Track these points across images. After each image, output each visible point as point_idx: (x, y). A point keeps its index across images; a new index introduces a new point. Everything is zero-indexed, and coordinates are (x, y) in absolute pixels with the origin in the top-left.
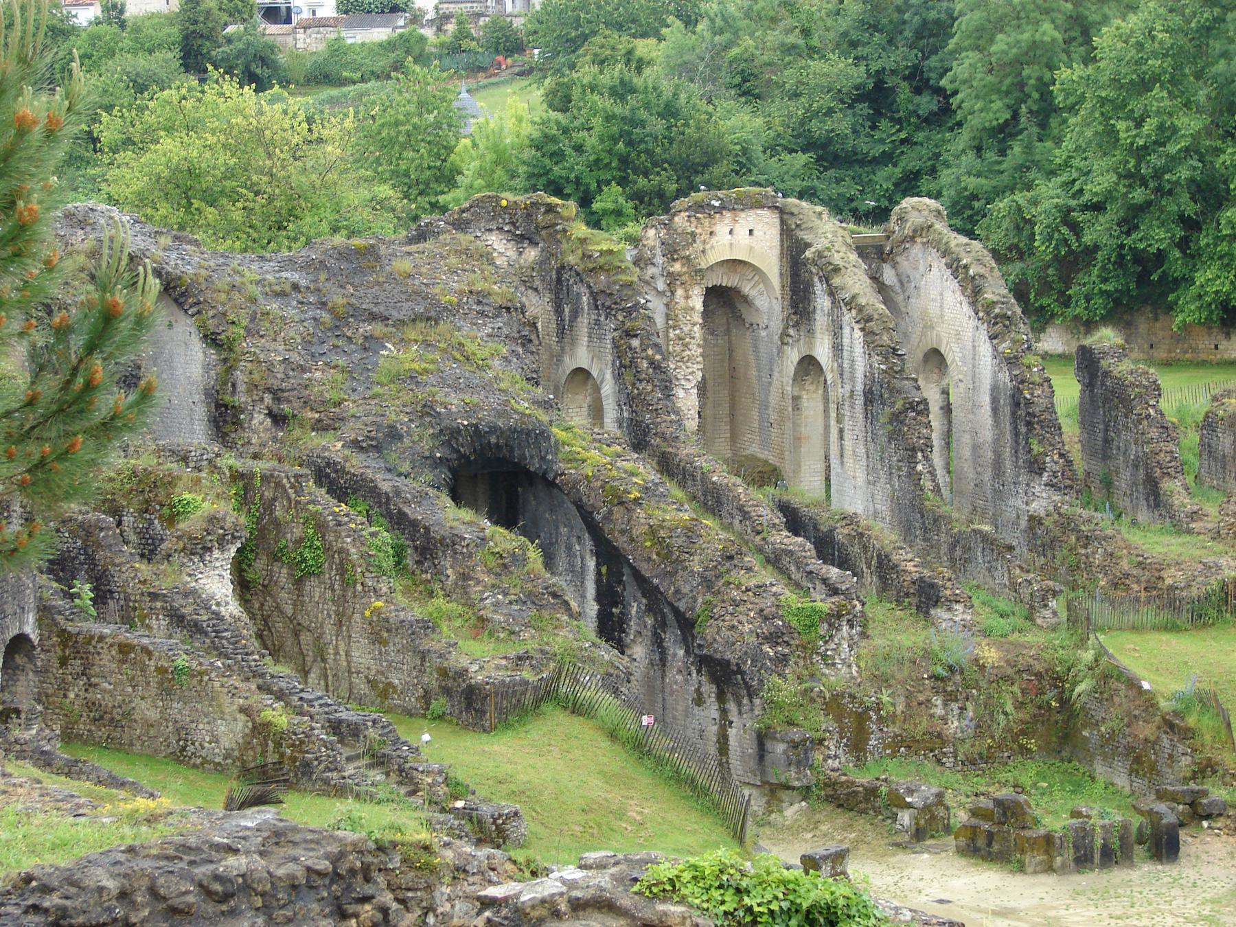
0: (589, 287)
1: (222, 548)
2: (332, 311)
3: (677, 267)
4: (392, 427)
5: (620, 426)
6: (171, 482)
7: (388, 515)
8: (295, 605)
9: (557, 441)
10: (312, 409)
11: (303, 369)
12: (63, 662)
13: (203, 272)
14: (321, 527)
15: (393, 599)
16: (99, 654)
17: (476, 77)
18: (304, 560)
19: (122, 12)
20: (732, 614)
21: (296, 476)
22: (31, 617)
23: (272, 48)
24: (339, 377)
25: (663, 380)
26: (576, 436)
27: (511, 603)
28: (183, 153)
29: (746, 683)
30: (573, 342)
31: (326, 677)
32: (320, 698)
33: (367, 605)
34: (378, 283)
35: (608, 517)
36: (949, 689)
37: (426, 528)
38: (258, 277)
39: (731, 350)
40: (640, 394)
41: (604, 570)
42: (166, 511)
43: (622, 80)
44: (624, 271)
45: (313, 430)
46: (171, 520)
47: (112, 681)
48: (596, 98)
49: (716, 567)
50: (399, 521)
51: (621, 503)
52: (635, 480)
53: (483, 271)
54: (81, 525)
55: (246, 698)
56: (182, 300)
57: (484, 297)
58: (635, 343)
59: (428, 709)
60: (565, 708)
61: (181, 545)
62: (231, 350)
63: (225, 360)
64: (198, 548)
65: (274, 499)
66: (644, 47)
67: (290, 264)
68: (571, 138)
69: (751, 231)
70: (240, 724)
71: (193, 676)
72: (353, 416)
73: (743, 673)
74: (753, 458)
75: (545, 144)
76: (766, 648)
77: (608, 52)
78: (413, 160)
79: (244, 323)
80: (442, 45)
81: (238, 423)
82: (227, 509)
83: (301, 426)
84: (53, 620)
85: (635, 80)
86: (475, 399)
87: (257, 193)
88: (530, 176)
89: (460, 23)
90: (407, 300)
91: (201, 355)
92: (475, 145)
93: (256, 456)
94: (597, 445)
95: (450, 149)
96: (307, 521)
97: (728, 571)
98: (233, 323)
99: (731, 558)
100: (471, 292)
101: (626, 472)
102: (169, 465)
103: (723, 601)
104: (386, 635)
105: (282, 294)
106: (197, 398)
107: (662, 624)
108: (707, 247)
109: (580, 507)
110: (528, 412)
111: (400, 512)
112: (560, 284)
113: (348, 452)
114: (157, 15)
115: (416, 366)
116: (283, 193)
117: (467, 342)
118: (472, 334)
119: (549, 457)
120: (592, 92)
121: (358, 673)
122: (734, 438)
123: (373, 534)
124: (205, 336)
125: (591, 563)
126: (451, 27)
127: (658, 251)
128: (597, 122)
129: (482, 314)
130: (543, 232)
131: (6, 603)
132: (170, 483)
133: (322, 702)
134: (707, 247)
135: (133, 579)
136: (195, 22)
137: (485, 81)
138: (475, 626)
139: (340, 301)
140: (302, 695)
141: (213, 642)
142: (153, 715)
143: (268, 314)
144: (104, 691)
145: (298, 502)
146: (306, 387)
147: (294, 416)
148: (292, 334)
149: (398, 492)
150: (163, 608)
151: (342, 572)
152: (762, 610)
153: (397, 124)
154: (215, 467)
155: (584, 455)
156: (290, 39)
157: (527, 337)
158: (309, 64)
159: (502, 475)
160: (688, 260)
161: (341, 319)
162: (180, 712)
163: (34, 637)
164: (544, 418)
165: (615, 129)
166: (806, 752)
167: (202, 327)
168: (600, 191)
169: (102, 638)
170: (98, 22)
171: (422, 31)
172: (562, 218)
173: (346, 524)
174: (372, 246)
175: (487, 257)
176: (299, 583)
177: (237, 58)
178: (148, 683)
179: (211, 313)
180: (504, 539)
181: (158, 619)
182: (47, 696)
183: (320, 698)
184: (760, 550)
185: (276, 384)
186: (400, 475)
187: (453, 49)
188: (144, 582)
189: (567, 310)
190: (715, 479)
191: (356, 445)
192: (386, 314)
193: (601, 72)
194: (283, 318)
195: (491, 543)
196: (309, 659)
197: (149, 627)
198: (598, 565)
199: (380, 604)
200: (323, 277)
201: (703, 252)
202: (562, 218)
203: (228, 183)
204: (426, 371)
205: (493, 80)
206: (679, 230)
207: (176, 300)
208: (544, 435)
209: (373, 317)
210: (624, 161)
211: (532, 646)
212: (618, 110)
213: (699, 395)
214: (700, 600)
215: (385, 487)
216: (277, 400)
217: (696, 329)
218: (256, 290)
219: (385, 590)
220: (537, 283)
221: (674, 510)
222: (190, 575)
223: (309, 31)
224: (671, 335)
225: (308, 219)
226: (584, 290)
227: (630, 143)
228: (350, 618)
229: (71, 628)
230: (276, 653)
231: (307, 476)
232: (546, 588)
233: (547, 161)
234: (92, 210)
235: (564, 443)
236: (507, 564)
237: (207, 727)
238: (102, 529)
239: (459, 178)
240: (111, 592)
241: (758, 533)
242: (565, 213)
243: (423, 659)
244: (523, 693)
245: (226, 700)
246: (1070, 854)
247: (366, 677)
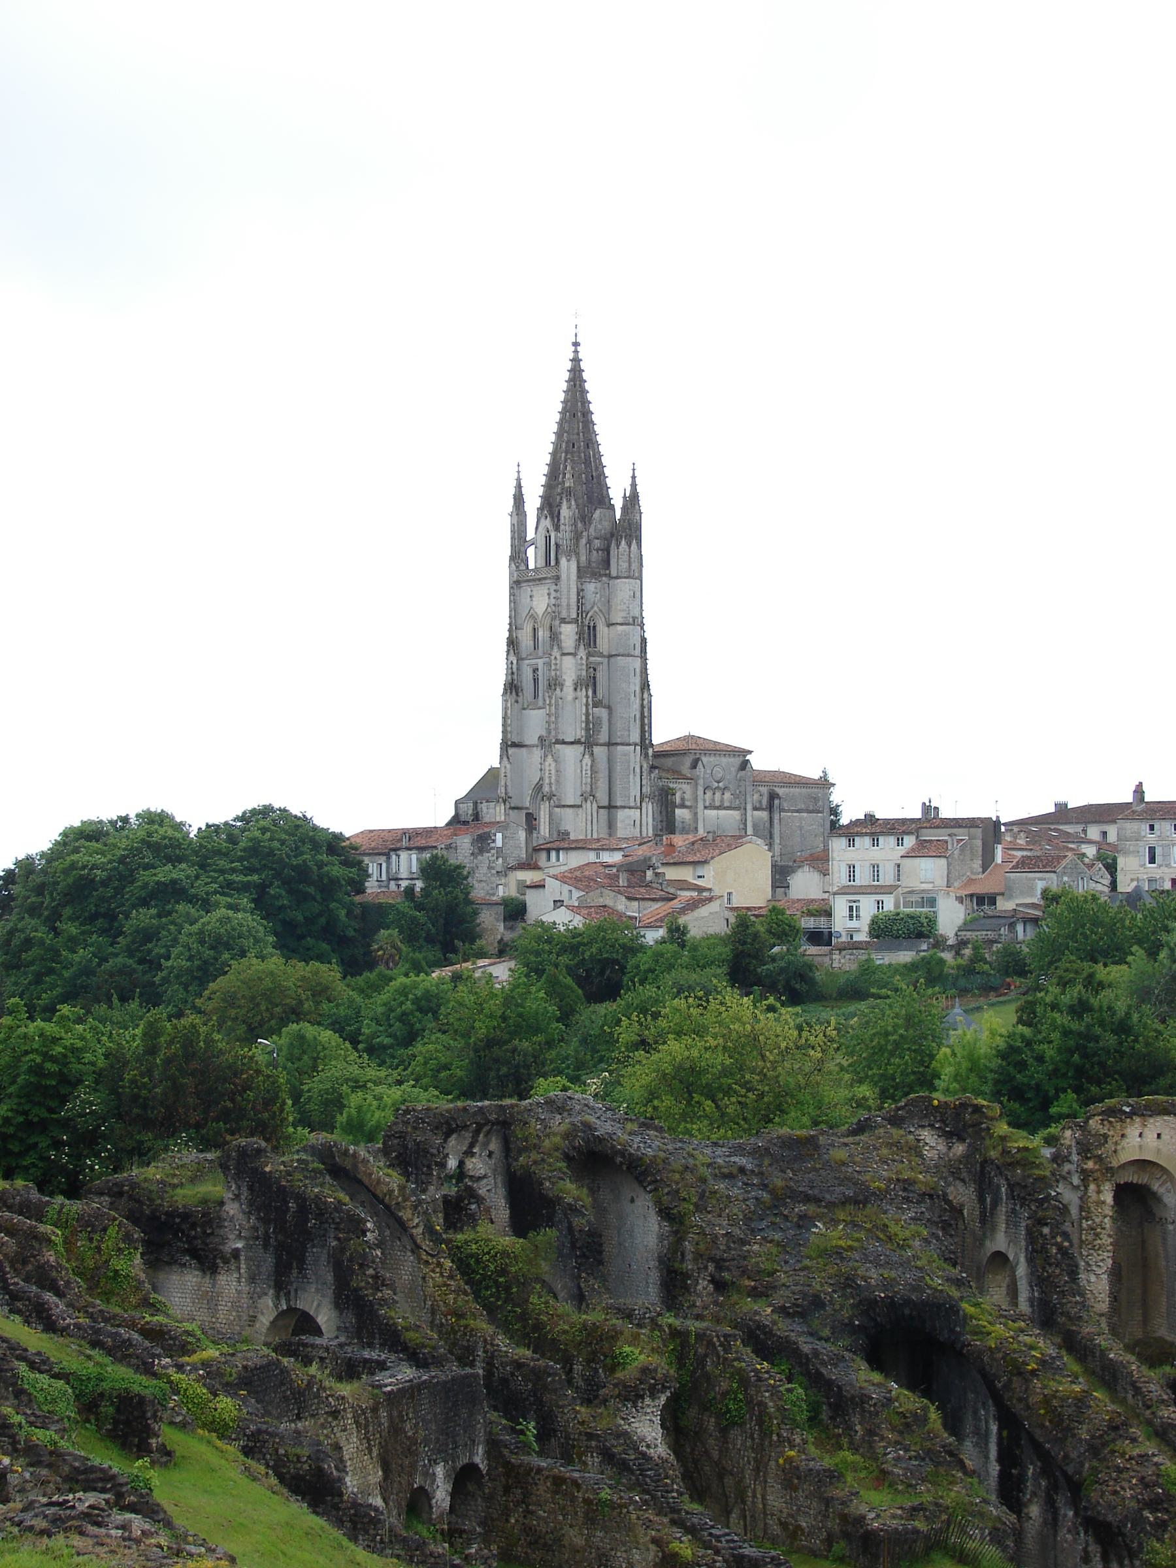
0: (1007, 1179)
1: (653, 1397)
2: (772, 1192)
3: (1090, 1165)
4: (816, 1296)
5: (1032, 1306)
6: (614, 1336)
7: (807, 1374)
8: (720, 1451)
9: (965, 1315)
10: (749, 1278)
11: (744, 1242)
12: (507, 1490)
13: (662, 1154)
14: (744, 1382)
15: (806, 1451)
16: (536, 1484)
17: (987, 996)
18: (729, 1411)
19: (684, 933)
20: (1115, 1480)
21: (725, 1336)
22: (480, 1450)
23: (810, 967)
24: (774, 1250)
25: (1069, 1265)
26: (983, 1311)
27: (910, 1458)
28: (687, 1053)
29: (1126, 1545)
30: (994, 1228)
31: (745, 1517)
32: (728, 1534)
33: (782, 1454)
34: (814, 1169)
35: (1008, 1386)
37: (839, 1387)
38: (709, 1161)
39: (1143, 1242)
40: (1049, 1277)
41: (1005, 1434)
42: (609, 1361)
43: (1080, 1000)
44: (1038, 1166)
45: (749, 1296)
46: (612, 1369)
47: (547, 1509)
48: (1056, 1015)
49: (1101, 1436)
50: (816, 1381)
51: (1020, 1374)
52: (1033, 1353)
53: (910, 1162)
54: (533, 1370)
55: (658, 1530)
56: (642, 1178)
57: (910, 1184)
58: (1046, 1230)
59: (830, 1551)
60: (953, 1557)
61: (617, 1391)
62: (682, 1223)
63: (676, 1232)
64: (632, 1395)
65: (706, 1355)
66: (1102, 972)
67: (739, 1150)
68: (1032, 1050)
69: (1159, 1136)
70: (652, 1554)
71: (613, 1508)
72: (784, 1285)
73: (1124, 1535)
74: (1161, 1340)
75: (1010, 1054)
76: (1147, 1514)
77: (1072, 975)
78: (899, 1066)
79: (694, 1200)
80: (959, 967)
81: (686, 1288)
82: (662, 1364)
83: (739, 1292)
84: (500, 1453)
85: (1092, 1000)
86: (893, 1274)
87: (749, 1090)
88: (996, 1082)
89: (975, 948)
90: (840, 1185)
91: (656, 1227)
92: (954, 1054)
93: (699, 1317)
94: (1003, 1320)
95: (932, 1057)
96: (732, 1376)
97: (1114, 1440)
98: (684, 1199)
99: (1116, 1428)
100: (898, 1180)
101: (1025, 1345)
102: (614, 1321)
103: (1108, 1468)
104: (796, 1481)
105: (730, 1176)
106: (652, 1264)
107: (1054, 1488)
108: (1119, 1147)
109: (984, 1374)
110: (940, 1288)
111: (817, 1370)
112: (982, 1175)
113: (775, 1317)
114: (715, 936)
115: (842, 1243)
116: (770, 1091)
117: (891, 1224)
118: (897, 1217)
119: (958, 1329)
120: (1052, 1010)
121: (772, 1515)
122: (1145, 1321)
123: (789, 1391)
124: (660, 1210)
125: (994, 1428)
126: (967, 952)
127: (1074, 1150)
128: (1056, 1036)
129: (907, 1200)
130: (970, 1130)
131: (458, 1435)
132: (612, 1337)
133: (728, 1538)
134: (1119, 1147)
135: (573, 1419)
136: (745, 943)
137: (994, 1000)
138: (877, 1479)
139: (779, 1183)
140: (713, 1531)
141: (638, 1479)
142: (579, 1541)
143: (715, 1192)
144: (539, 1518)
145: (726, 1359)
146: (745, 1258)
147: (733, 1283)
148: (735, 1211)
149: (816, 1353)
150: (597, 1447)
151: (760, 1423)
152: (1143, 1478)
153: (887, 1034)
154: (656, 1324)
155: (990, 1328)
156: (827, 959)
157: (948, 1218)
158: (842, 981)
159: (915, 1341)
160: (1099, 1159)
161: (780, 1199)
162: (602, 1541)
163: (483, 1467)
164: (955, 1293)
165: (1072, 1043)
167: (658, 1202)
168: (1057, 1097)
169: (539, 1470)
170: (663, 941)
171: (943, 955)
172: (987, 1118)
173: (766, 1380)
174: (812, 1137)
175: (916, 1149)
176: (724, 1431)
177: (779, 974)
178: (576, 1513)
179: (666, 1190)
180: (909, 1400)
181: (592, 1457)
182: (493, 1520)
183: (728, 1534)
184: (1149, 1423)
186: (820, 1339)
187: (968, 971)
188: (583, 1423)
189: (988, 1200)
190: (1111, 1356)
191: (782, 1310)
192: (820, 1196)
193: (1063, 993)
194: (728, 1197)
195: (897, 1404)
196: (731, 1501)
197: (585, 1463)
198: (1000, 1429)
199: (792, 1453)
200: (766, 1162)
201: (1115, 1151)
202: (987, 1118)
203: (724, 1080)
204: (851, 1248)
205: (1001, 999)
206: (1093, 1132)
207: (637, 1178)
208: (954, 1309)
209: (807, 1199)
210: (1080, 1071)
211: (927, 1498)
212: (1075, 1026)
213: (1111, 1283)
214: (1087, 1465)
215: (806, 1349)
216: (719, 1268)
217: (1106, 1220)
218: (706, 1172)
219: (798, 1441)
220: (964, 1175)
221: (1070, 1383)
222: (623, 1419)
223: (844, 953)
224: (1084, 1225)
225: (793, 1114)
226: (1003, 1182)
227: (1085, 1056)
228: (767, 1465)
229: (513, 1460)
230: (698, 1494)
231: (735, 1336)
232: (943, 1447)
233: (1011, 1069)
234: (570, 1098)
235: (972, 1317)
236: (910, 1423)
237: (624, 1555)
238: (549, 1375)
239: (937, 1082)
240: (555, 1431)
241: (1149, 1407)
242: (990, 1114)
243: (827, 1506)
244: (915, 1541)
245: (640, 1531)
247: (779, 1520)
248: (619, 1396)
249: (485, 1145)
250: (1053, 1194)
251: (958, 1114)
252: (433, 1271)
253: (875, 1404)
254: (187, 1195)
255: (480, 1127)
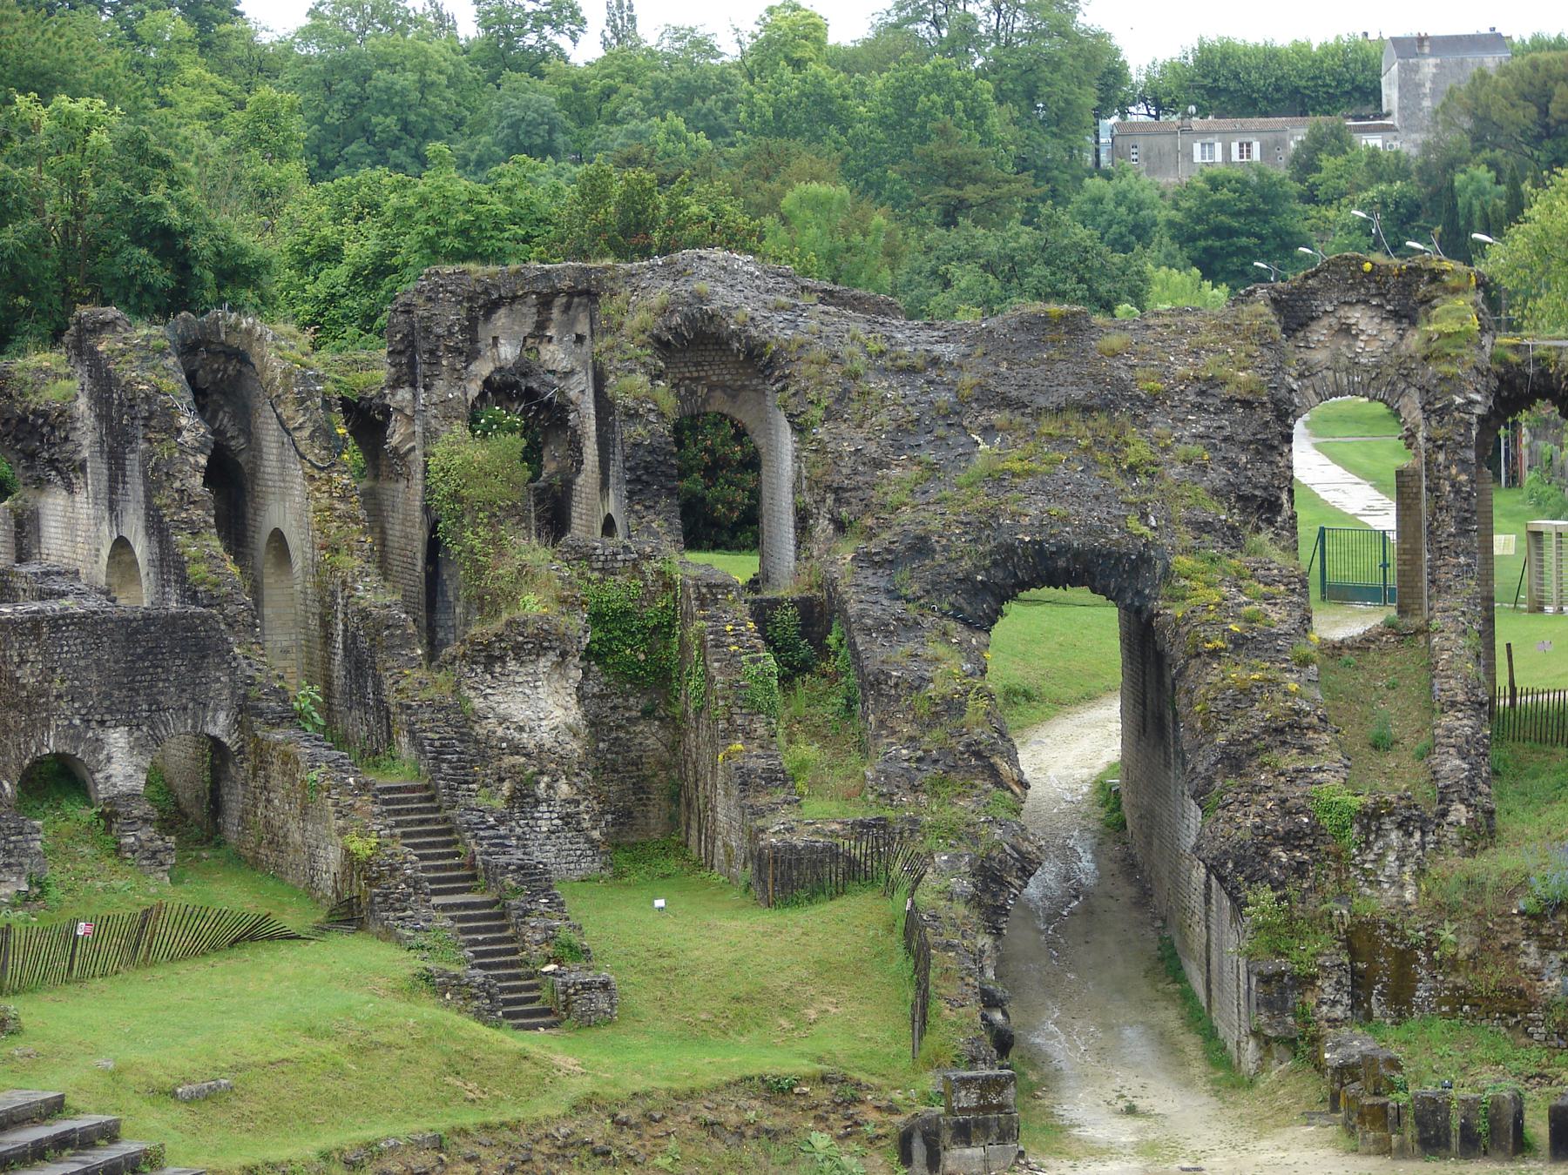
11: (877, 464)
36: (1544, 931)
49: (1249, 741)
97: (1267, 748)
100: (1197, 378)
152: (1284, 801)
166: (1282, 992)
185: (837, 480)
246: (1410, 1132)
248: (464, 655)
249: (569, 324)
250: (1459, 400)
251: (1407, 285)
252: (318, 490)
253: (897, 685)
254: (52, 394)
255: (545, 303)
